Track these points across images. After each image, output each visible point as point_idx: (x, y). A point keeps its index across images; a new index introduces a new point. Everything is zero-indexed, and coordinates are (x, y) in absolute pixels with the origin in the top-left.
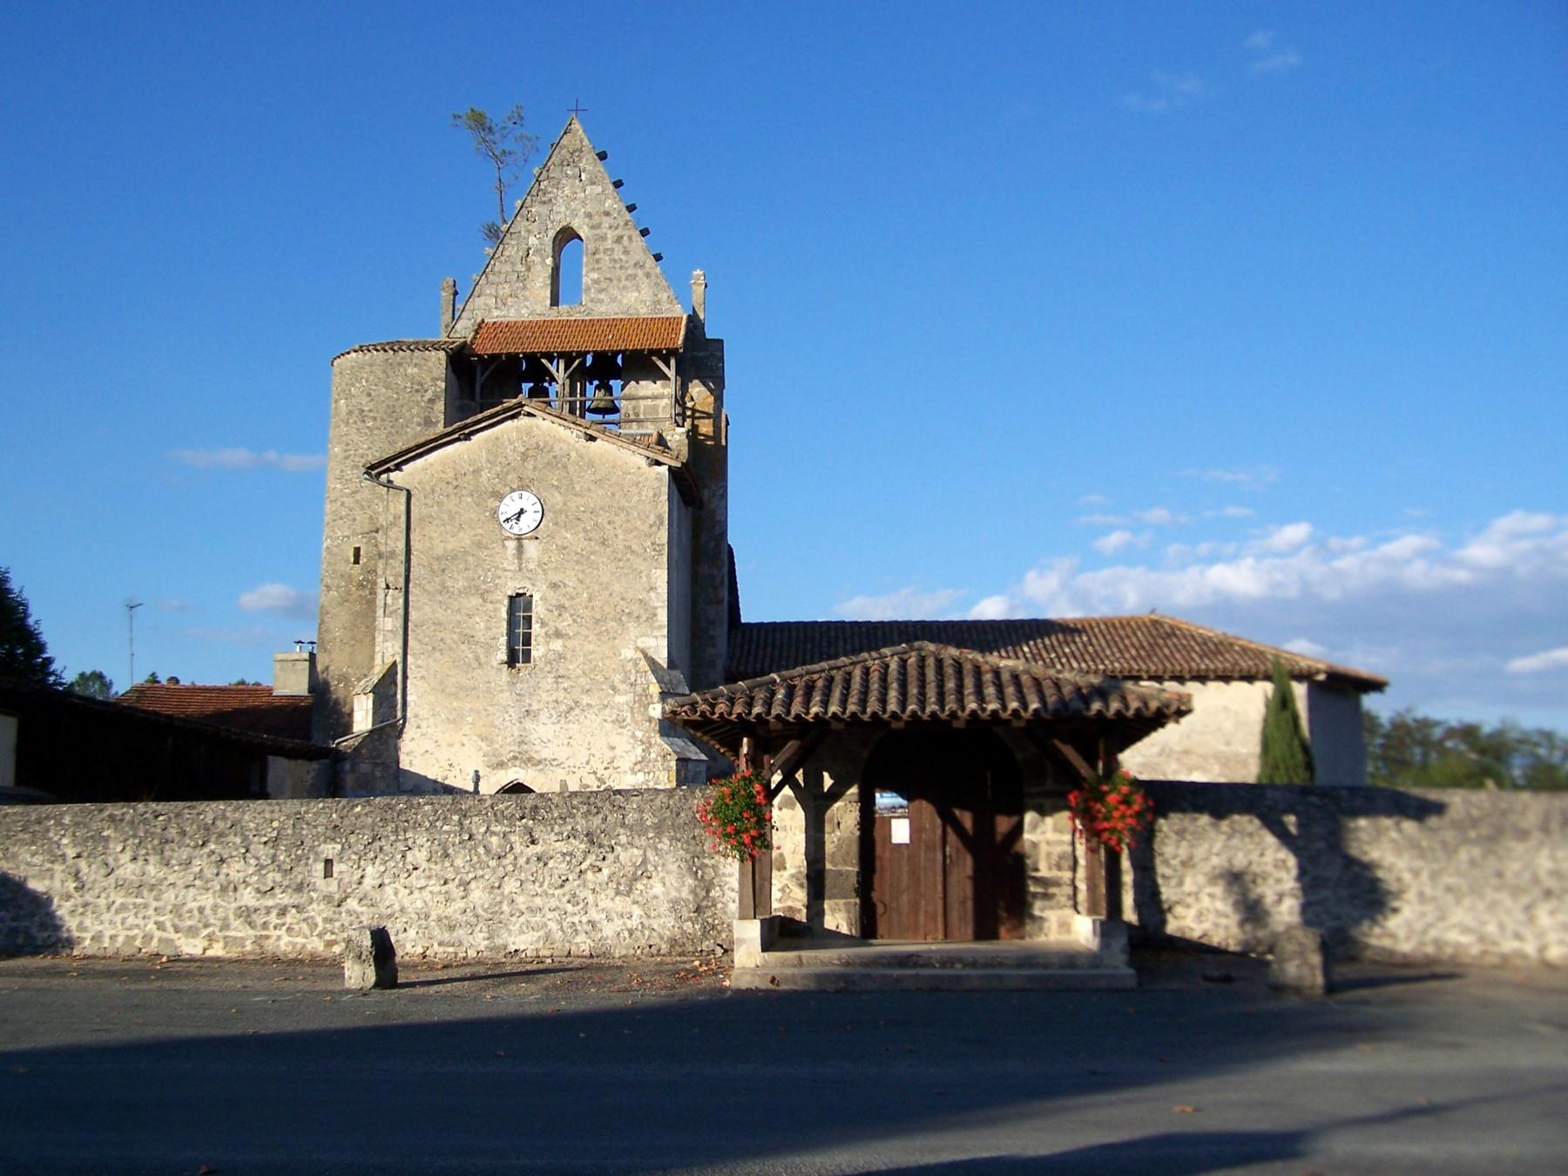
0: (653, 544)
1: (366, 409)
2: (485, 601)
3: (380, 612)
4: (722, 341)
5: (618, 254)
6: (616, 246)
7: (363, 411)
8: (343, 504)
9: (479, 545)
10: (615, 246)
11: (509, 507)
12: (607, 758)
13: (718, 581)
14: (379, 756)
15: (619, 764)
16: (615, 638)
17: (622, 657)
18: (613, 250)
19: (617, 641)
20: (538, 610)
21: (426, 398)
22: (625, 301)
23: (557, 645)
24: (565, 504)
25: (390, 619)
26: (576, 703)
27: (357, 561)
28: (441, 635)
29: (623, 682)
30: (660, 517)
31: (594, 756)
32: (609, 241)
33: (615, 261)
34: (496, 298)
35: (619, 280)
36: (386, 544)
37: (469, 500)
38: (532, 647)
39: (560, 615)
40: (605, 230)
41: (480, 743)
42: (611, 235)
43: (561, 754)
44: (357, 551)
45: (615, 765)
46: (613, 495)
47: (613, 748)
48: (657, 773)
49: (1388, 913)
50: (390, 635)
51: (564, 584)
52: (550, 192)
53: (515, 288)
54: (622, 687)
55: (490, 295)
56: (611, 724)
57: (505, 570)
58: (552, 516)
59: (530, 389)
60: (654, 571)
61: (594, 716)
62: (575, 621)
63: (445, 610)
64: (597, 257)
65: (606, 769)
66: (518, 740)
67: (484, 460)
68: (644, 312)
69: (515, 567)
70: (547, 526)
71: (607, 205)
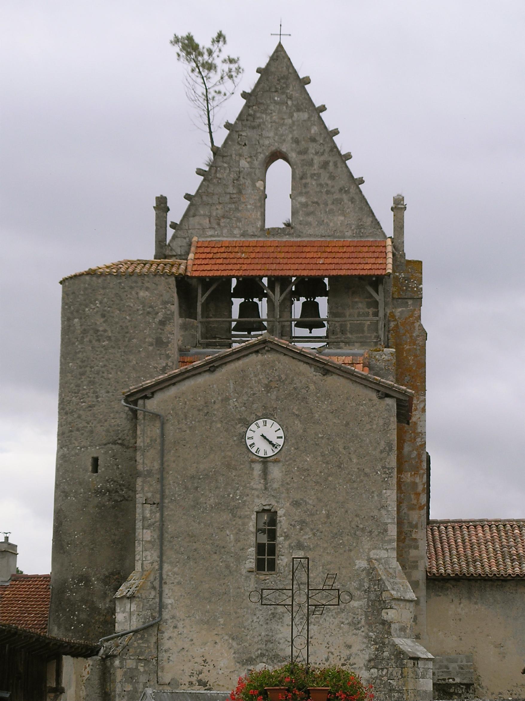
0: (383, 467)
1: (101, 329)
2: (234, 516)
3: (139, 525)
5: (324, 178)
7: (98, 331)
8: (79, 417)
9: (229, 466)
10: (321, 171)
14: (141, 653)
15: (354, 661)
16: (350, 550)
17: (357, 567)
18: (319, 175)
19: (352, 554)
21: (157, 320)
22: (331, 224)
24: (305, 431)
25: (149, 531)
27: (95, 469)
28: (195, 546)
29: (358, 589)
30: (389, 445)
31: (332, 653)
32: (316, 167)
33: (321, 185)
34: (210, 218)
35: (326, 204)
36: (143, 463)
37: (219, 425)
38: (276, 557)
39: (301, 529)
40: (311, 156)
41: (230, 641)
42: (317, 160)
44: (95, 461)
45: (352, 661)
46: (347, 424)
47: (350, 647)
48: (391, 669)
49: (191, 35)
50: (150, 545)
51: (305, 501)
52: (258, 118)
53: (227, 209)
54: (357, 593)
55: (204, 215)
56: (347, 626)
57: (253, 489)
58: (294, 441)
59: (241, 305)
60: (384, 491)
61: (332, 619)
62: (314, 534)
63: (199, 523)
64: (304, 181)
65: (343, 665)
66: (265, 639)
67: (232, 390)
69: (261, 486)
70: (289, 450)
71: (313, 131)
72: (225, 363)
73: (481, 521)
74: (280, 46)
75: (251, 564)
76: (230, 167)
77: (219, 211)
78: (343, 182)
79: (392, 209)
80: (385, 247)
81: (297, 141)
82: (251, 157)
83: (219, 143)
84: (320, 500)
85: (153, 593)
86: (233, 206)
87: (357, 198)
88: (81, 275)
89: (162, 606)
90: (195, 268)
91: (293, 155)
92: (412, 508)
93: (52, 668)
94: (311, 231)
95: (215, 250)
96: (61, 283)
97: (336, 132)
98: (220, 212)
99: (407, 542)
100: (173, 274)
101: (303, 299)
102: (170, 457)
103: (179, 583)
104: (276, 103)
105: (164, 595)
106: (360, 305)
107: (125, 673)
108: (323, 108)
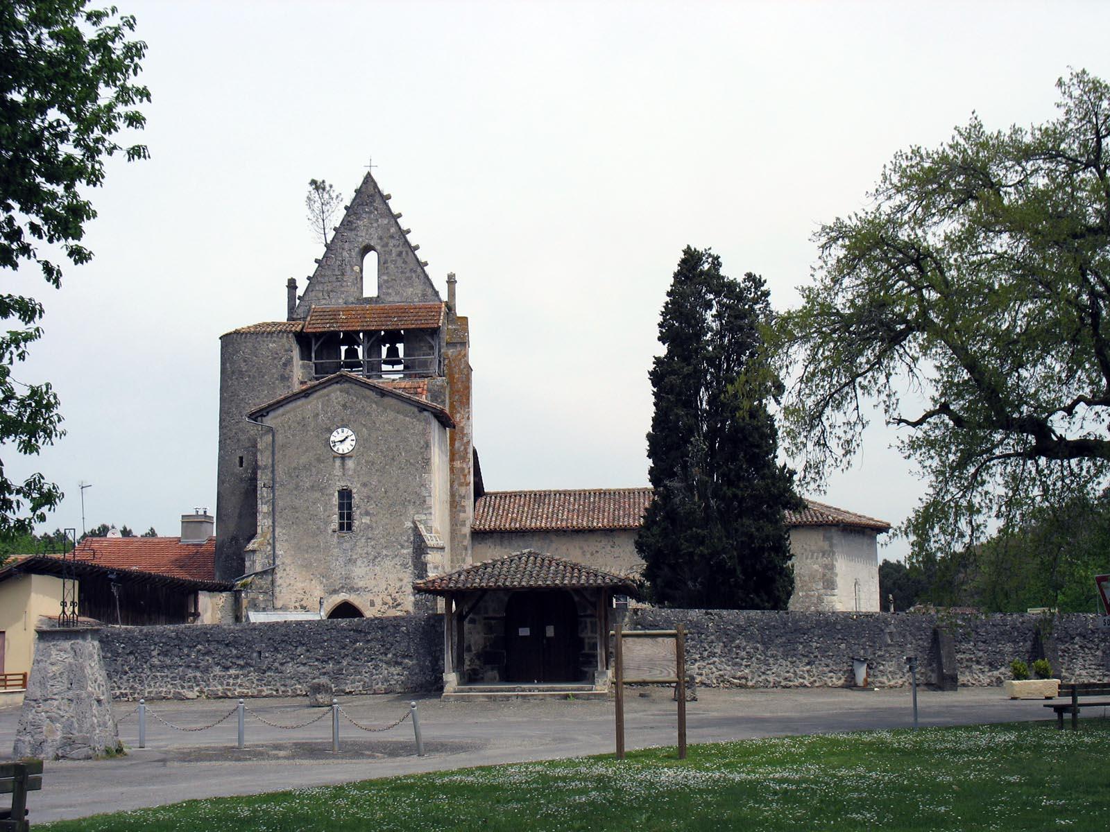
2: (323, 494)
3: (259, 502)
4: (467, 318)
6: (398, 258)
9: (319, 460)
11: (336, 436)
12: (398, 585)
13: (467, 471)
18: (396, 261)
20: (356, 499)
21: (281, 363)
22: (405, 294)
23: (366, 520)
24: (369, 435)
26: (379, 554)
29: (407, 541)
43: (371, 584)
44: (241, 458)
59: (346, 350)
62: (377, 505)
68: (417, 301)
69: (340, 474)
72: (316, 391)
73: (521, 492)
74: (369, 174)
75: (335, 525)
76: (336, 257)
77: (328, 287)
78: (412, 265)
79: (456, 282)
80: (440, 308)
81: (381, 238)
82: (350, 250)
83: (329, 239)
84: (380, 482)
85: (269, 548)
86: (338, 283)
87: (422, 275)
88: (230, 334)
89: (274, 556)
90: (310, 326)
91: (378, 248)
92: (461, 485)
93: (192, 598)
94: (391, 299)
95: (325, 313)
96: (220, 338)
97: (408, 231)
98: (330, 288)
99: (458, 508)
100: (291, 331)
101: (388, 345)
102: (278, 456)
103: (287, 540)
104: (366, 212)
105: (276, 549)
106: (424, 348)
107: (249, 602)
108: (400, 215)
